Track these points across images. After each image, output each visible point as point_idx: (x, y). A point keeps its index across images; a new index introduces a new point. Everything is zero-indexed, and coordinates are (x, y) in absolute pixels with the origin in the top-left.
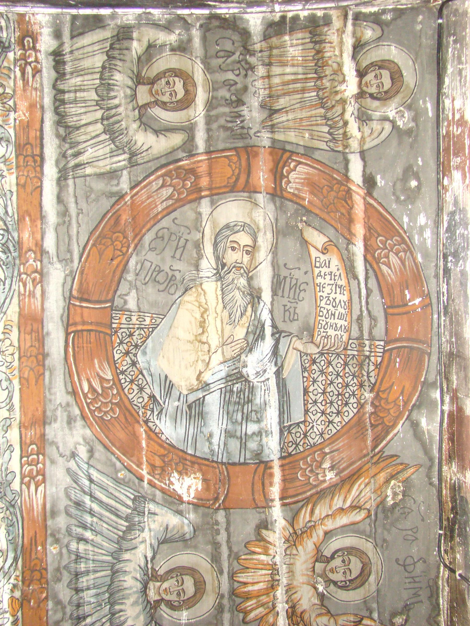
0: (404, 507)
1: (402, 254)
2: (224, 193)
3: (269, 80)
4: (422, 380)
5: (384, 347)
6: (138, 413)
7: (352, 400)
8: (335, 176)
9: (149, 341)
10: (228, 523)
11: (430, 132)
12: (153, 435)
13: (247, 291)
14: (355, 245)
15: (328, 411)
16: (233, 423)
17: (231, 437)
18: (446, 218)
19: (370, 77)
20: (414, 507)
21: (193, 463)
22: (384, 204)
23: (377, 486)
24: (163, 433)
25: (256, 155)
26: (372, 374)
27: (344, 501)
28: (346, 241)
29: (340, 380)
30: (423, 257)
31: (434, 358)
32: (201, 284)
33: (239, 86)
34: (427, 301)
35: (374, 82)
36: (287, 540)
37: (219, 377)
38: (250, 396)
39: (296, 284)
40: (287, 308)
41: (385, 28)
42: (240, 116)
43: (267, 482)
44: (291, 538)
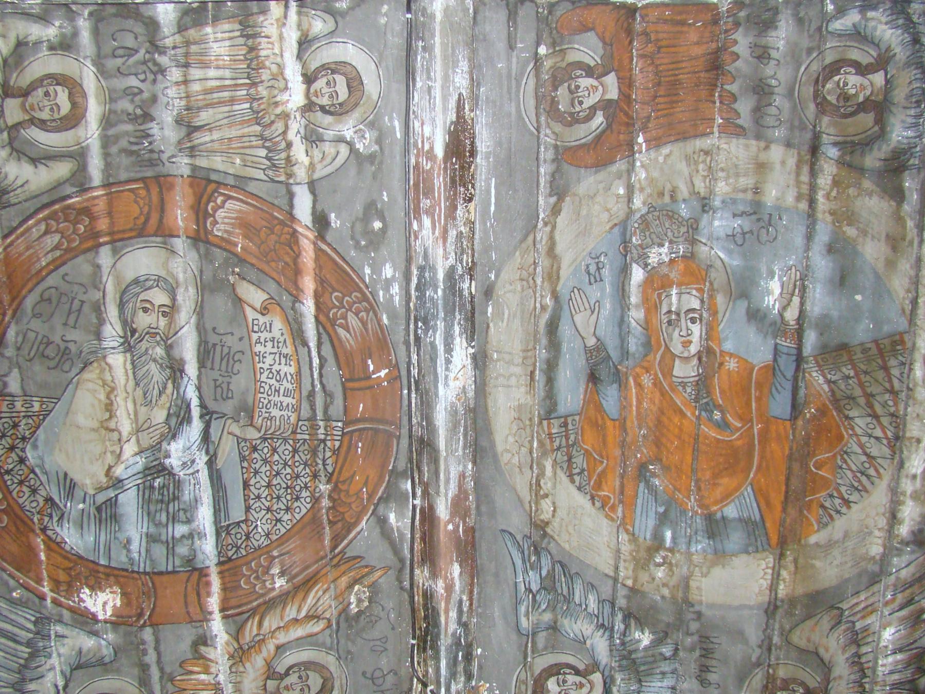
0: (371, 615)
1: (363, 314)
2: (131, 238)
3: (187, 87)
4: (390, 468)
5: (343, 429)
6: (32, 520)
7: (305, 494)
8: (276, 214)
9: (40, 432)
10: (157, 641)
11: (398, 158)
12: (53, 545)
13: (166, 362)
14: (303, 304)
15: (275, 507)
16: (156, 525)
17: (155, 541)
18: (415, 272)
19: (320, 84)
20: (382, 614)
21: (108, 575)
22: (340, 251)
23: (338, 591)
24: (66, 543)
25: (171, 187)
26: (329, 461)
27: (299, 611)
28: (290, 298)
29: (289, 470)
30: (388, 318)
31: (405, 442)
32: (105, 357)
33: (146, 95)
34: (396, 373)
35: (326, 90)
36: (232, 657)
37: (135, 471)
38: (176, 492)
39: (229, 353)
40: (218, 383)
41: (339, 19)
42: (149, 135)
43: (203, 592)
44: (236, 654)
